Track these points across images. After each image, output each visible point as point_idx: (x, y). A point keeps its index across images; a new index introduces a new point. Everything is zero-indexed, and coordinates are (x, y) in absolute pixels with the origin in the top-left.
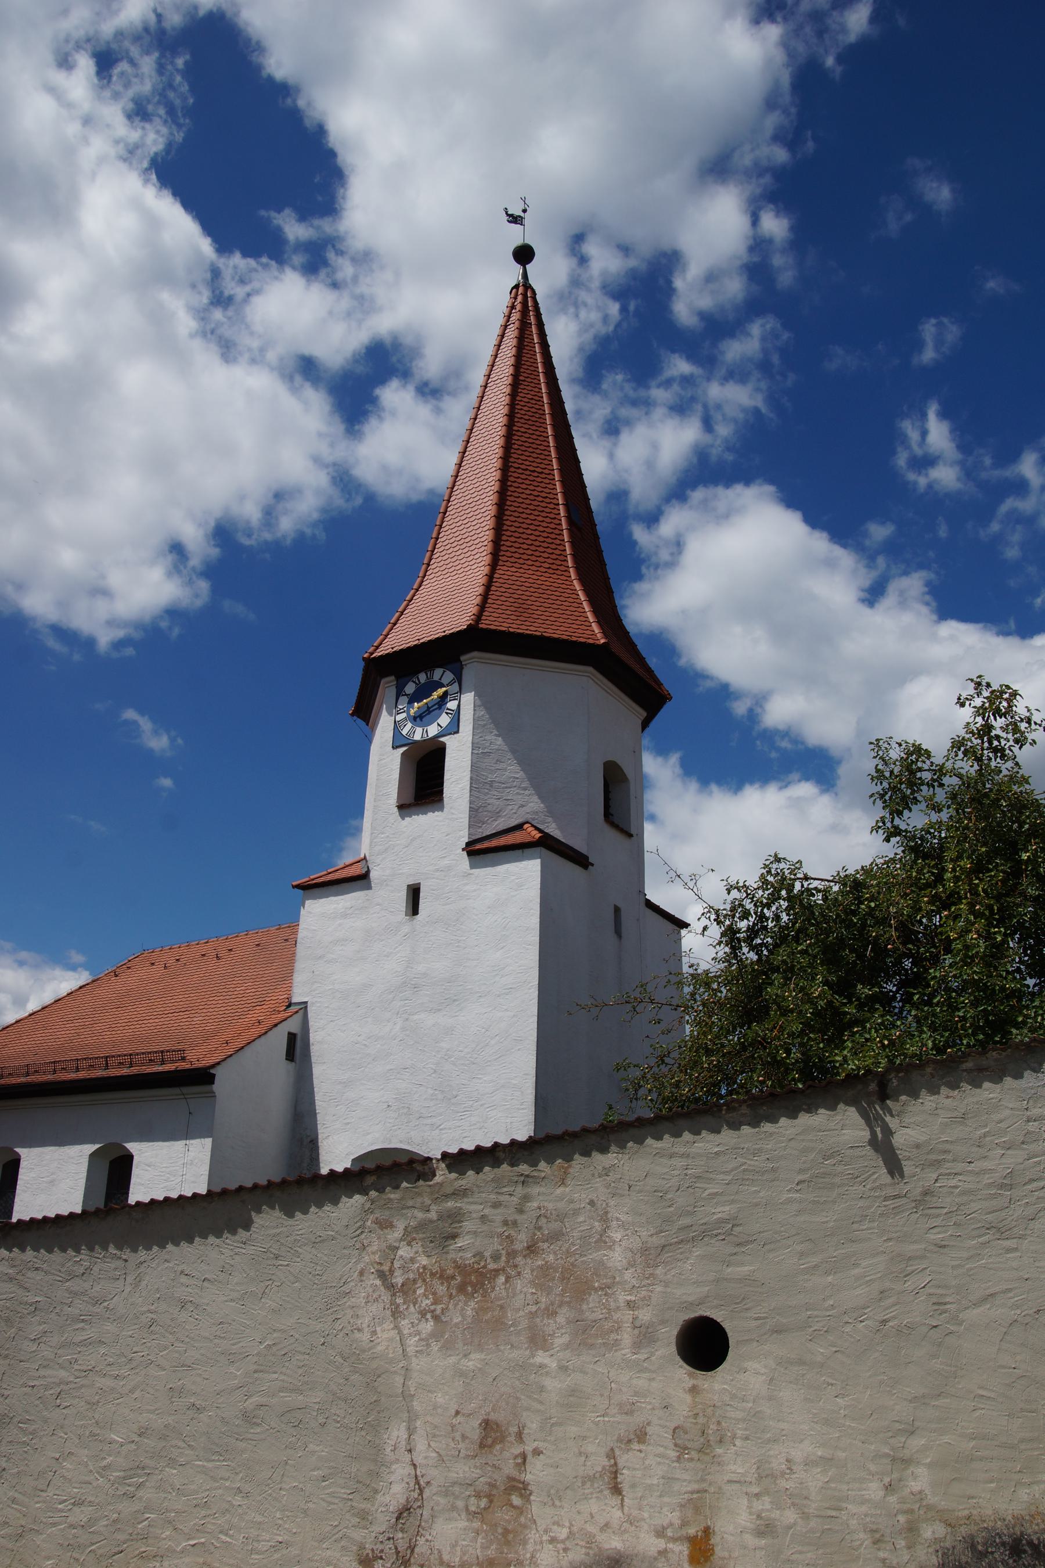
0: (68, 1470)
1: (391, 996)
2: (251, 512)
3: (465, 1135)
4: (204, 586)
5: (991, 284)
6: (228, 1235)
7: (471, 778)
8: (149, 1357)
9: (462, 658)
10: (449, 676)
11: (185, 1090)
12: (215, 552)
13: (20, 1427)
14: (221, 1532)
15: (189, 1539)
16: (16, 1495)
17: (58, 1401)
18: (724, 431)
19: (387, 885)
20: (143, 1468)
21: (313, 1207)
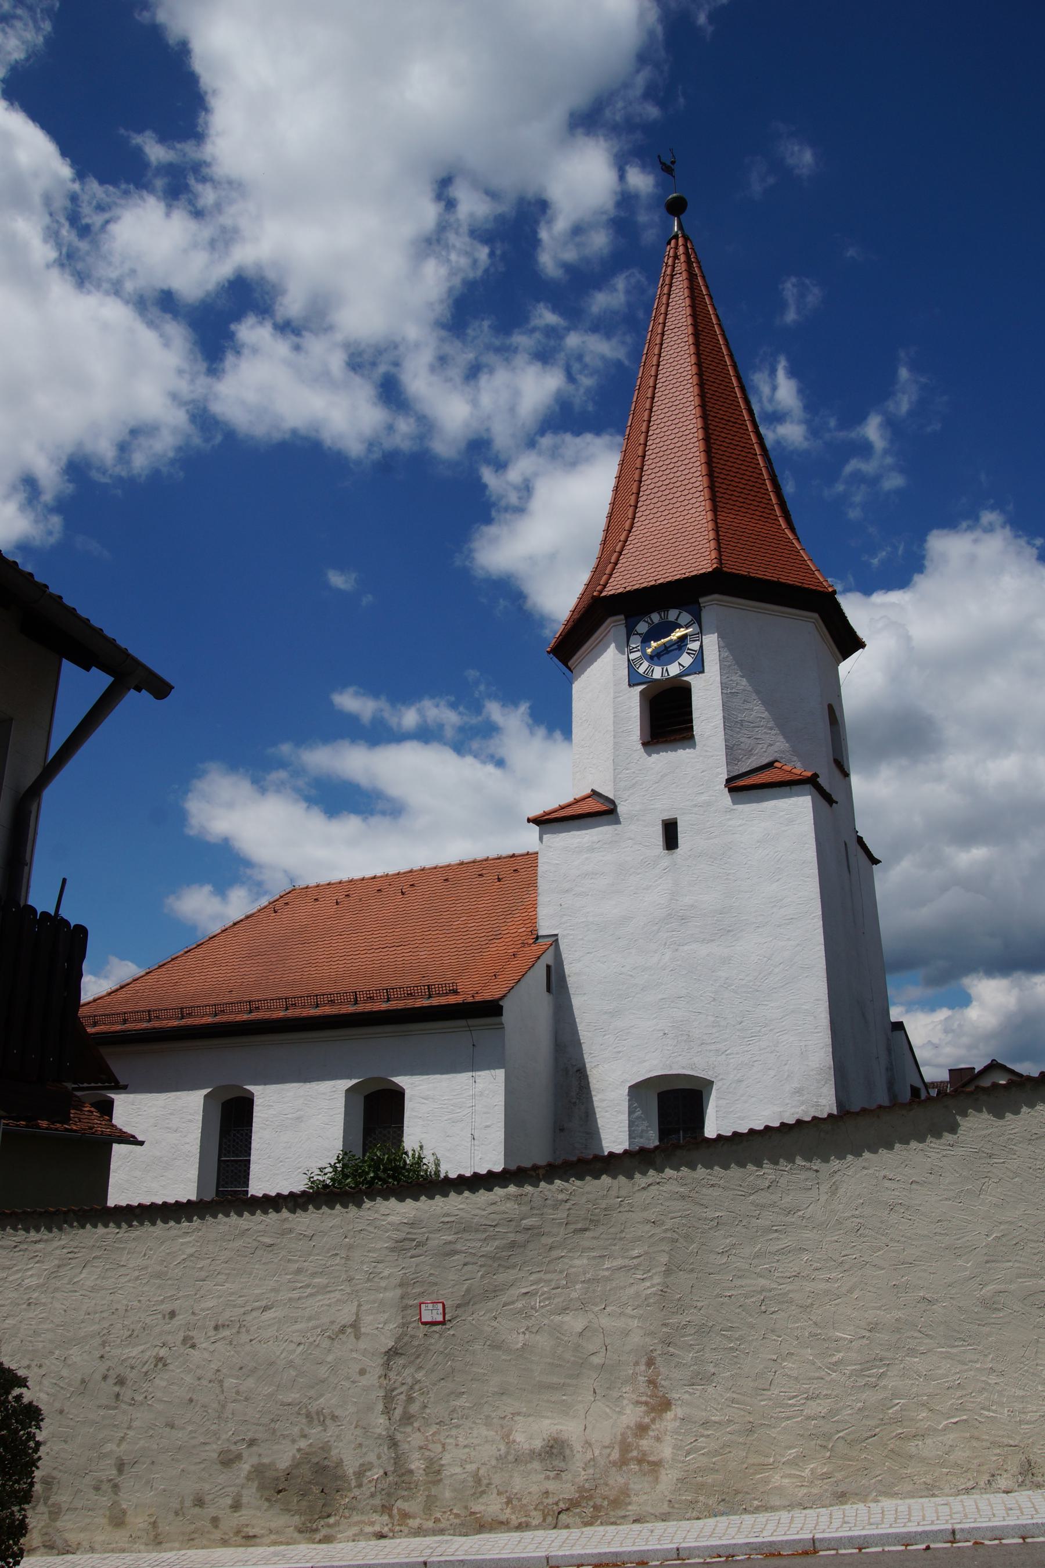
0: (791, 1369)
1: (655, 928)
2: (105, 449)
3: (755, 1059)
4: (56, 521)
5: (851, 253)
6: (934, 1140)
7: (724, 717)
8: (863, 1259)
9: (701, 600)
10: (685, 617)
11: (471, 1022)
12: (70, 488)
13: (722, 1335)
14: (983, 1409)
15: (949, 1418)
16: (735, 1396)
17: (763, 1308)
18: (587, 382)
19: (638, 820)
20: (881, 1360)
21: (1025, 1108)
